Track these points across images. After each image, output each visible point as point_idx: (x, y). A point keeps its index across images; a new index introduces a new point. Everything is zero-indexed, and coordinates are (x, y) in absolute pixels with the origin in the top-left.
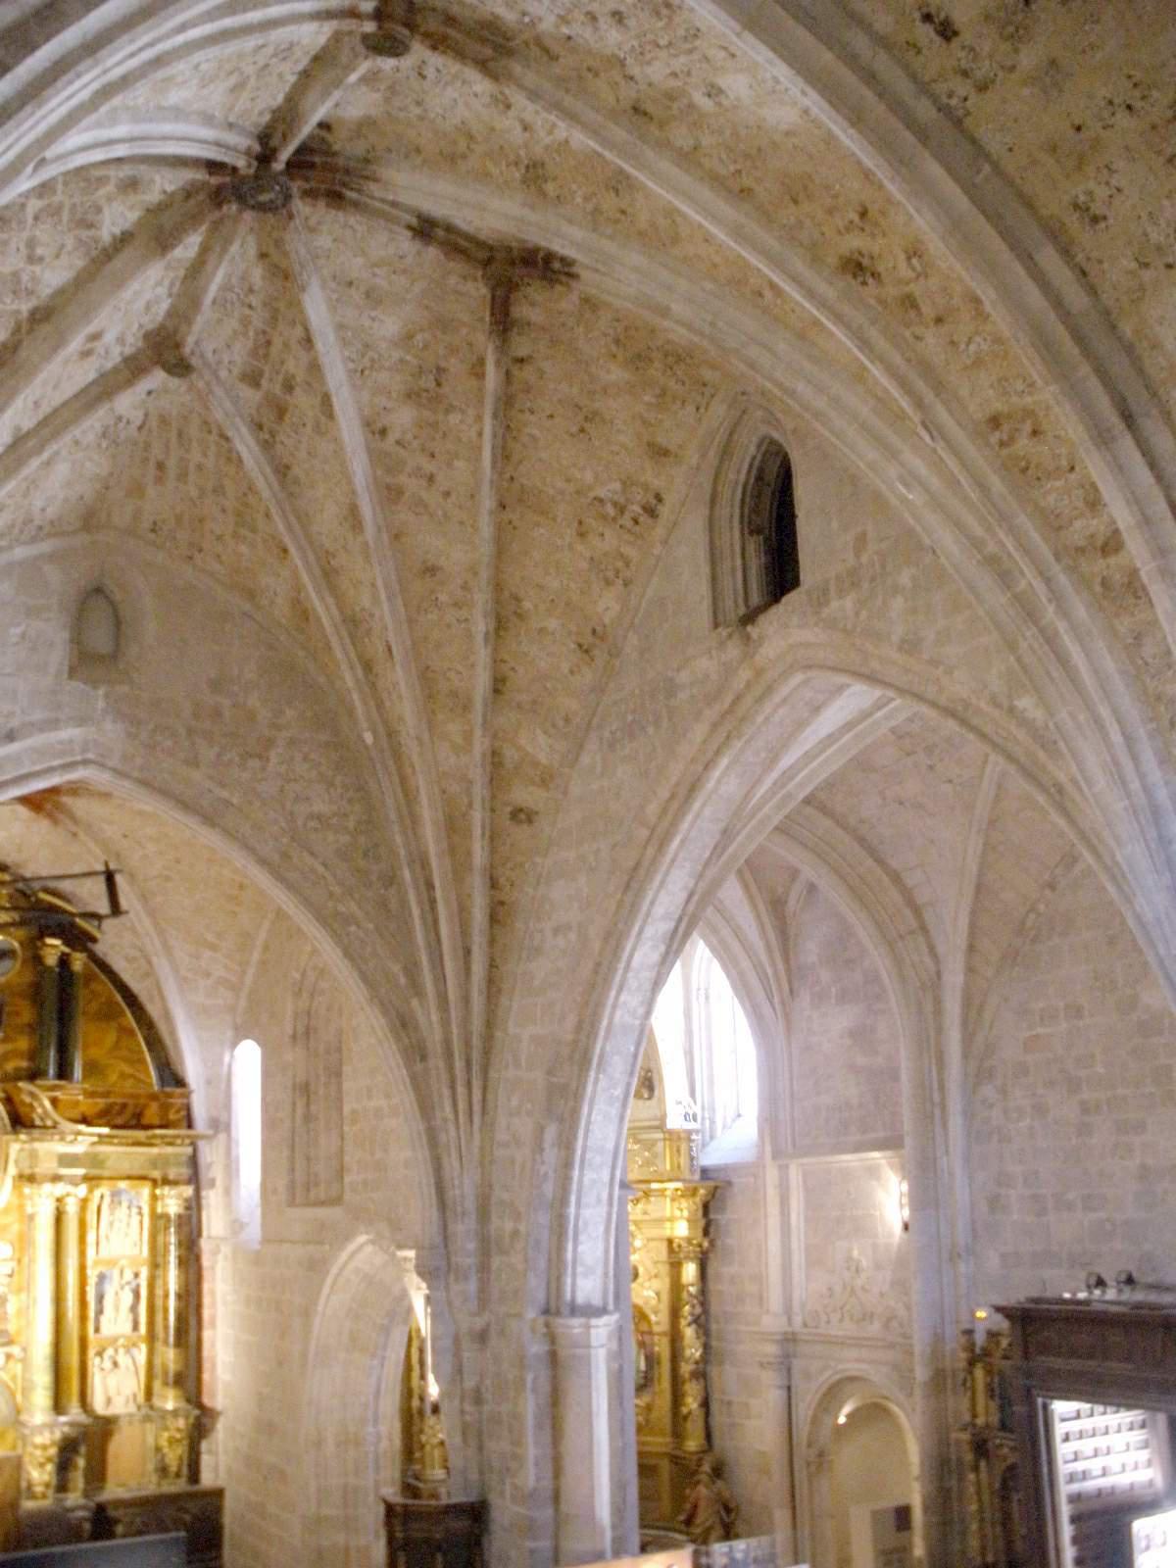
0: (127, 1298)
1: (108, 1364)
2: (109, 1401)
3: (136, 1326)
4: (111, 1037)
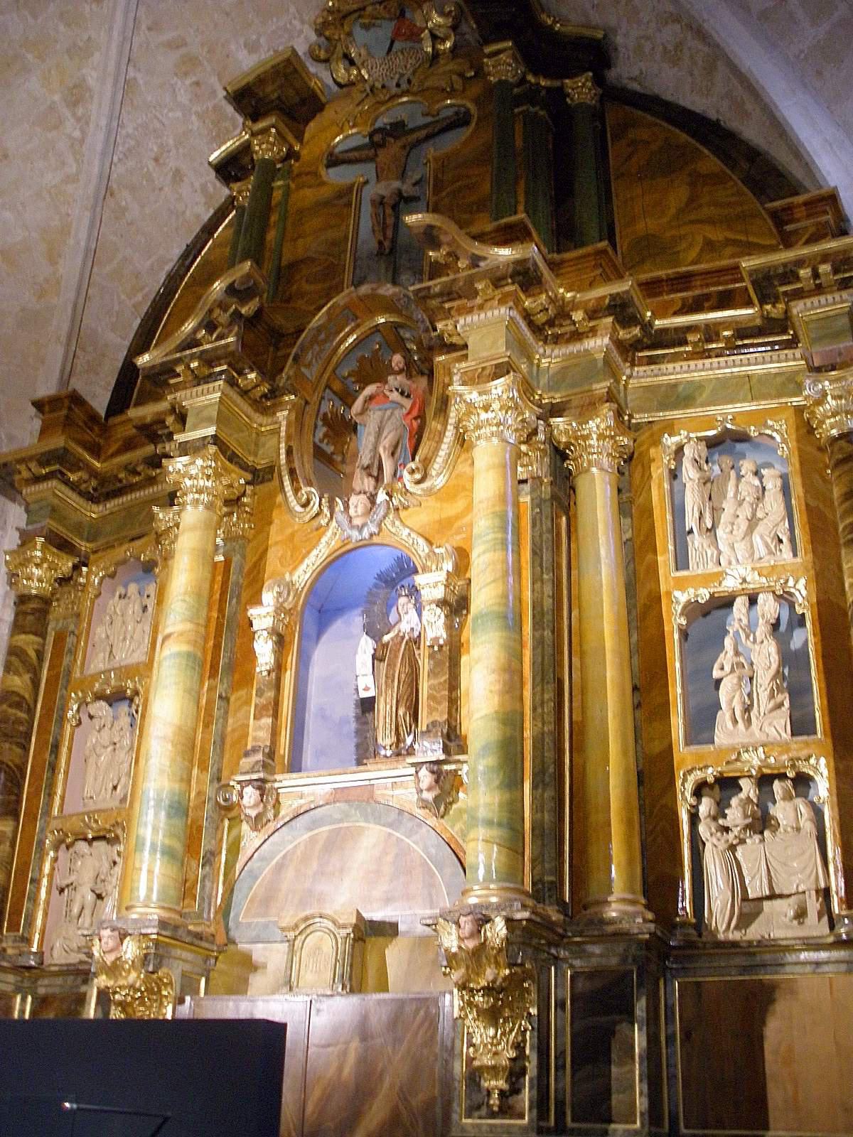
0: (766, 655)
1: (735, 815)
2: (749, 909)
3: (801, 726)
4: (678, 195)
